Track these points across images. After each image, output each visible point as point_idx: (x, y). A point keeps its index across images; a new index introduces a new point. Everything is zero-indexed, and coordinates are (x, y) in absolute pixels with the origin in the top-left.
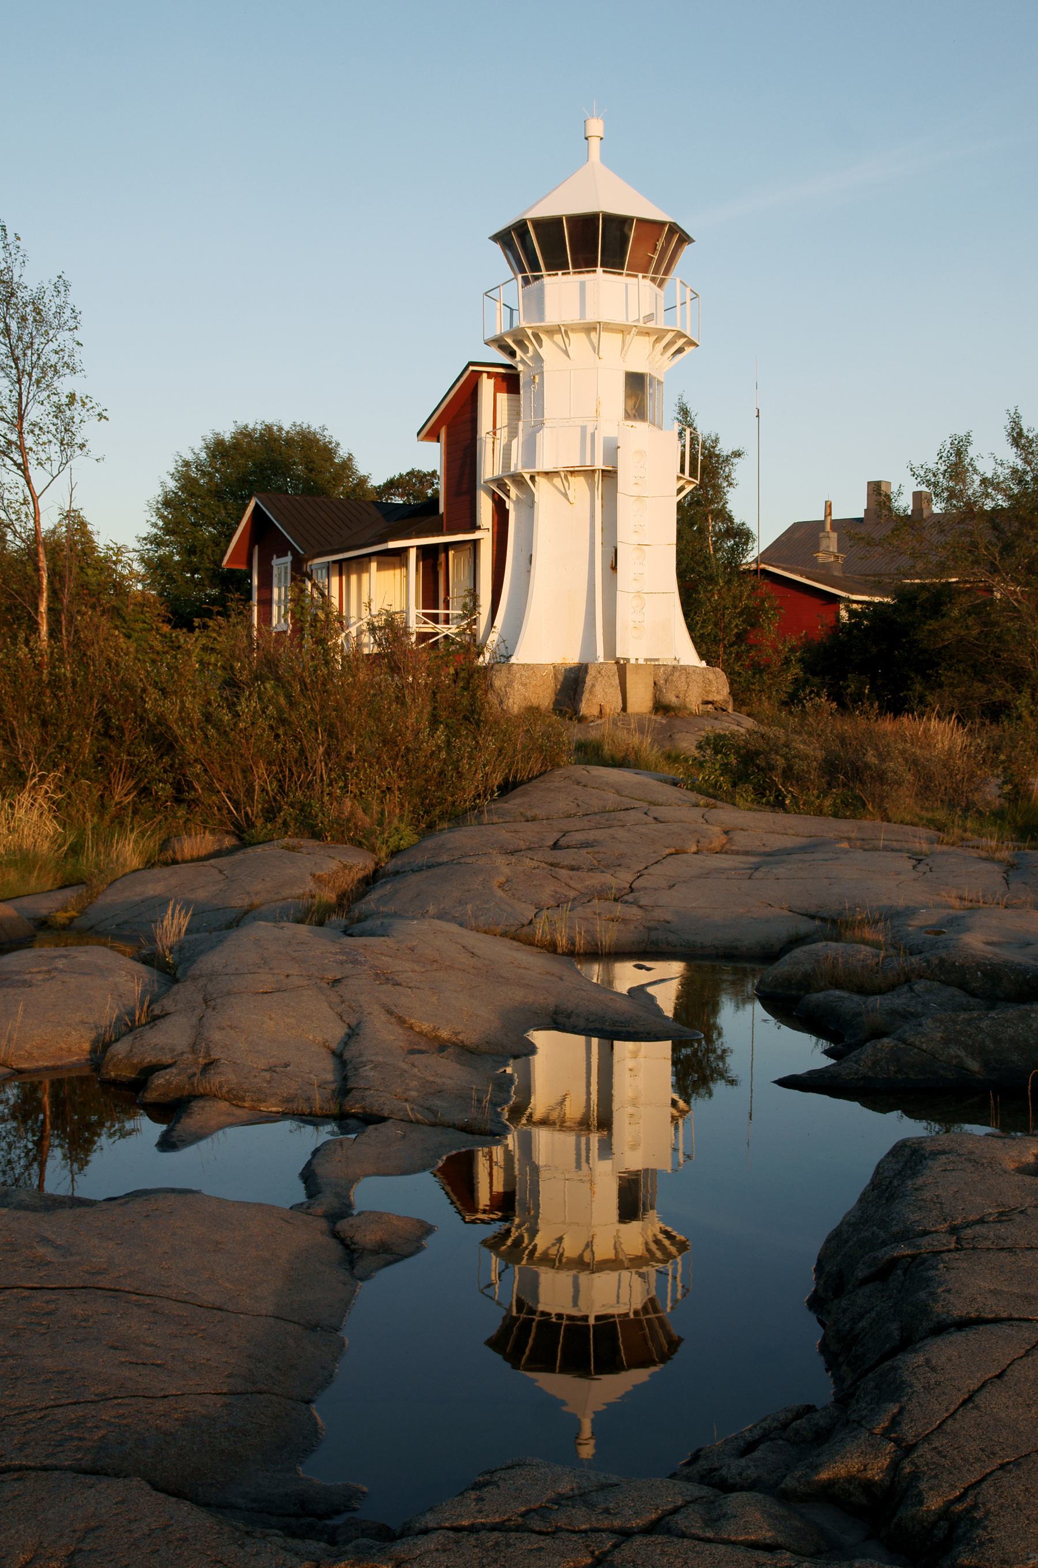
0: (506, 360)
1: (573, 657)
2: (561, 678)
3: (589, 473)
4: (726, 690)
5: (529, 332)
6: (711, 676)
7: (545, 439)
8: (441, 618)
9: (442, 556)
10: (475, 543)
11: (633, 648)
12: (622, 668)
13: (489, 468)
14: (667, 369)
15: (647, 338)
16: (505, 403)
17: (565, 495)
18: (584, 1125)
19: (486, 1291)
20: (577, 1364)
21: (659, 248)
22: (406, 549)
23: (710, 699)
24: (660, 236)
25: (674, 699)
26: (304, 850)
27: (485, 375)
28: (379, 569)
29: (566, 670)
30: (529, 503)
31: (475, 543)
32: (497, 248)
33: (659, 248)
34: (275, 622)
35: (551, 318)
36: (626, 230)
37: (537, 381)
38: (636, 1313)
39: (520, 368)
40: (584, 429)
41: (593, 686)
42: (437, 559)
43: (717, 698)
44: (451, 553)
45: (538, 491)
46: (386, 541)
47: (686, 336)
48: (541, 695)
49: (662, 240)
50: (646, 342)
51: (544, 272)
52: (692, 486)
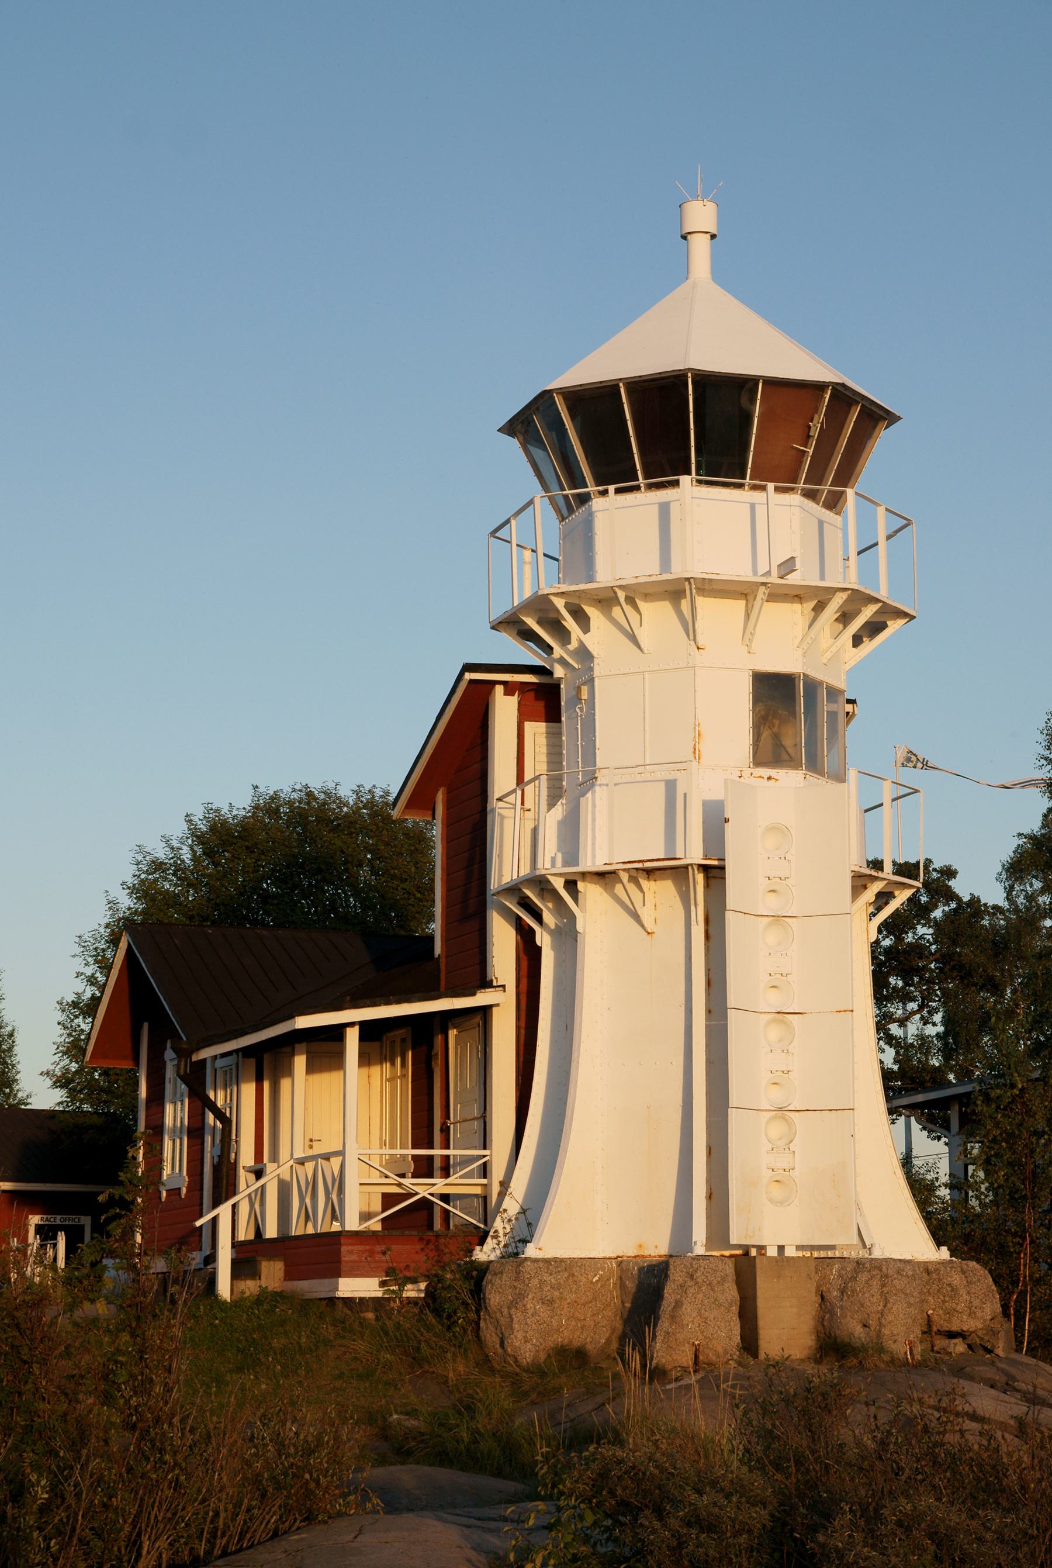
0: (526, 655)
1: (657, 1244)
2: (631, 1286)
3: (678, 873)
4: (992, 1306)
5: (559, 603)
6: (956, 1279)
7: (598, 806)
8: (437, 1164)
9: (439, 1039)
10: (485, 1011)
11: (774, 1222)
12: (746, 1265)
13: (507, 865)
14: (853, 663)
15: (797, 606)
16: (542, 741)
17: (636, 917)
21: (815, 433)
22: (337, 1033)
23: (955, 1327)
24: (816, 410)
25: (858, 1330)
27: (499, 689)
28: (310, 1069)
29: (641, 1269)
30: (568, 936)
31: (485, 1011)
32: (513, 444)
33: (815, 433)
34: (167, 1172)
35: (605, 575)
36: (744, 401)
37: (585, 696)
38: (604, 493)
39: (559, 672)
40: (671, 786)
41: (678, 1304)
42: (431, 1046)
43: (969, 1325)
44: (452, 1033)
45: (583, 910)
46: (291, 1017)
47: (877, 601)
48: (589, 1322)
49: (820, 418)
50: (797, 613)
51: (592, 488)
52: (908, 893)
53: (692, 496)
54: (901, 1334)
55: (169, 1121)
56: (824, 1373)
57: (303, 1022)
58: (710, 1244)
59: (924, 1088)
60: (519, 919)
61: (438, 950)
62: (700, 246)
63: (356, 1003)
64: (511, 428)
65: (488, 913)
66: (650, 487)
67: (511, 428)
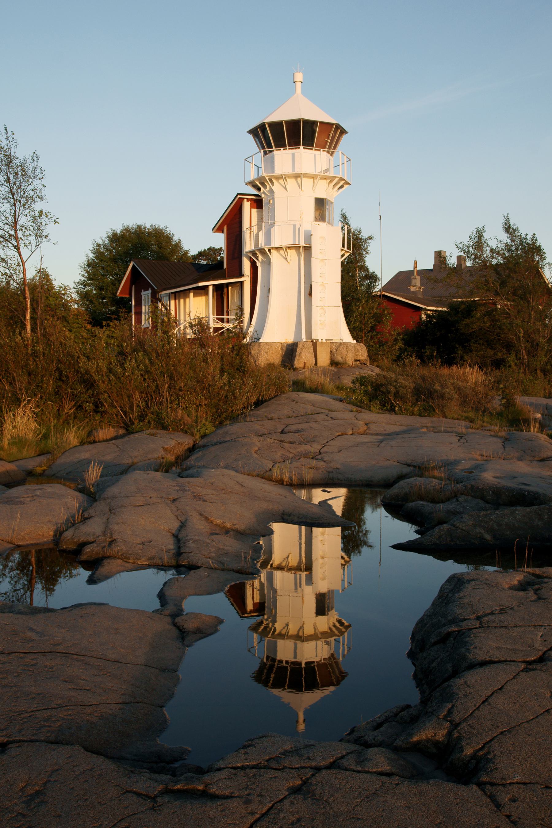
0: (256, 192)
1: (290, 339)
2: (284, 349)
3: (297, 248)
5: (267, 178)
6: (359, 348)
8: (225, 320)
10: (242, 283)
11: (320, 334)
12: (315, 344)
13: (248, 245)
16: (256, 214)
21: (331, 136)
22: (207, 287)
24: (331, 130)
25: (340, 359)
27: (245, 200)
28: (194, 296)
30: (268, 263)
32: (251, 137)
33: (331, 136)
35: (278, 171)
37: (271, 202)
39: (263, 196)
40: (294, 226)
41: (301, 353)
44: (230, 288)
45: (272, 257)
46: (198, 283)
50: (325, 183)
51: (274, 149)
52: (348, 254)
53: (302, 152)
54: (350, 360)
55: (143, 310)
56: (333, 369)
57: (201, 284)
58: (307, 338)
60: (251, 258)
61: (225, 266)
63: (213, 280)
64: (250, 132)
65: (243, 258)
66: (289, 149)
67: (250, 132)
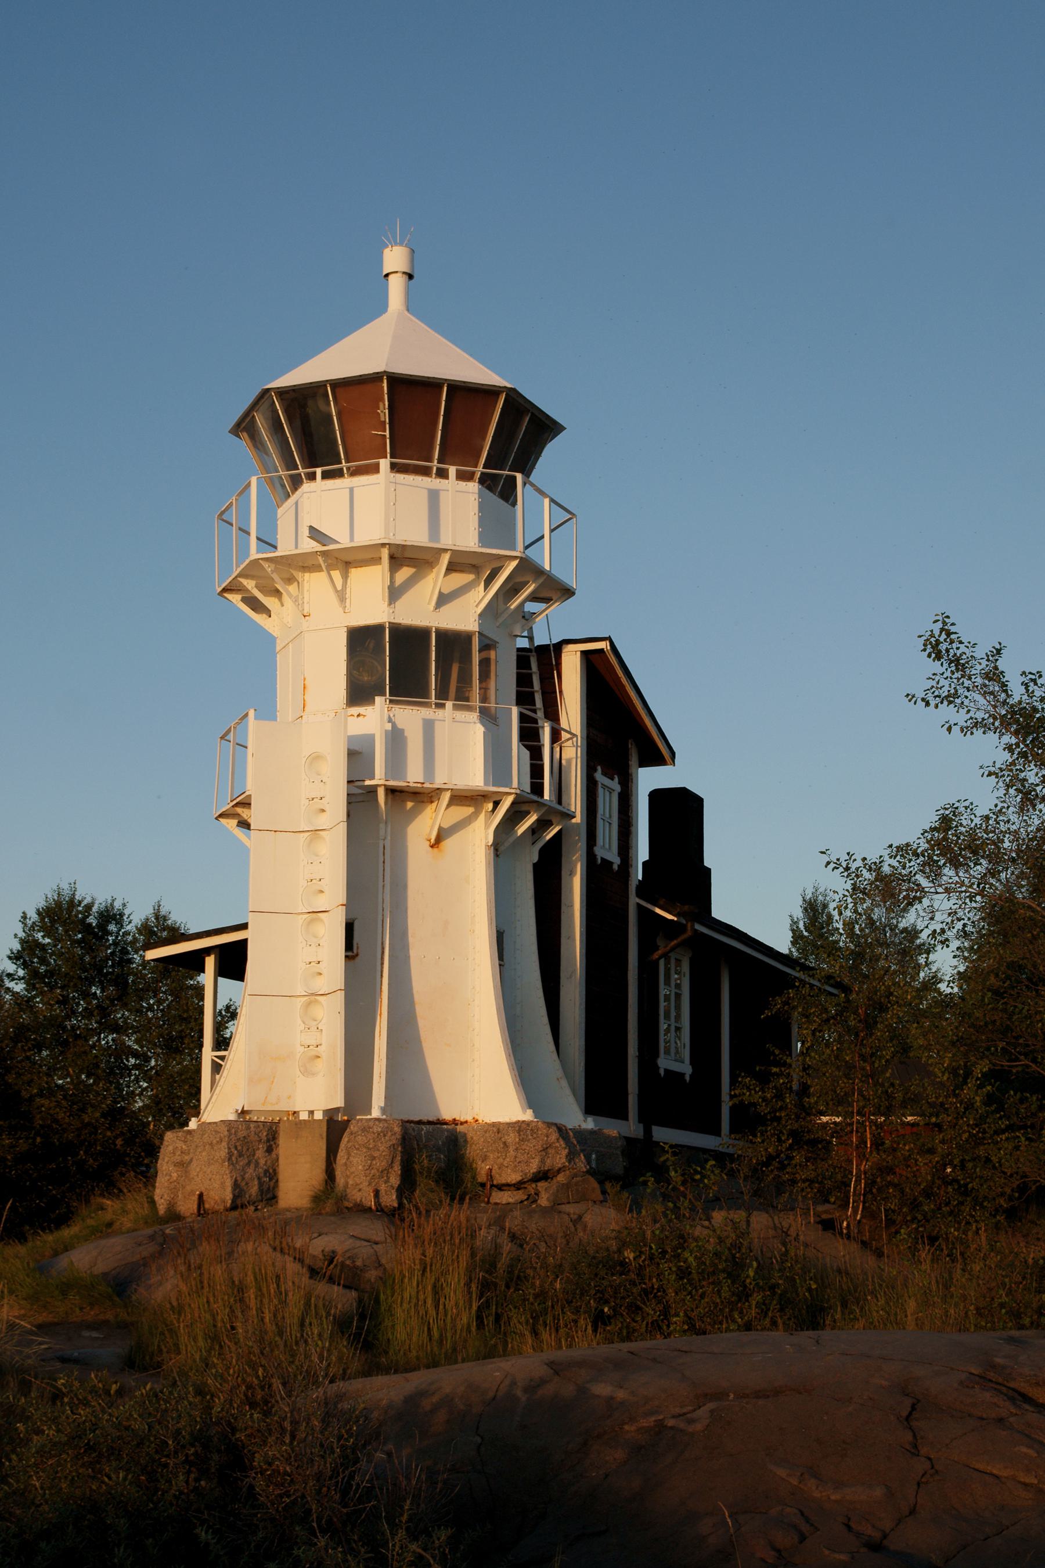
18: (408, 798)
19: (224, 517)
20: (408, 391)
26: (500, 1310)
38: (312, 477)
59: (274, 1188)
62: (396, 286)
